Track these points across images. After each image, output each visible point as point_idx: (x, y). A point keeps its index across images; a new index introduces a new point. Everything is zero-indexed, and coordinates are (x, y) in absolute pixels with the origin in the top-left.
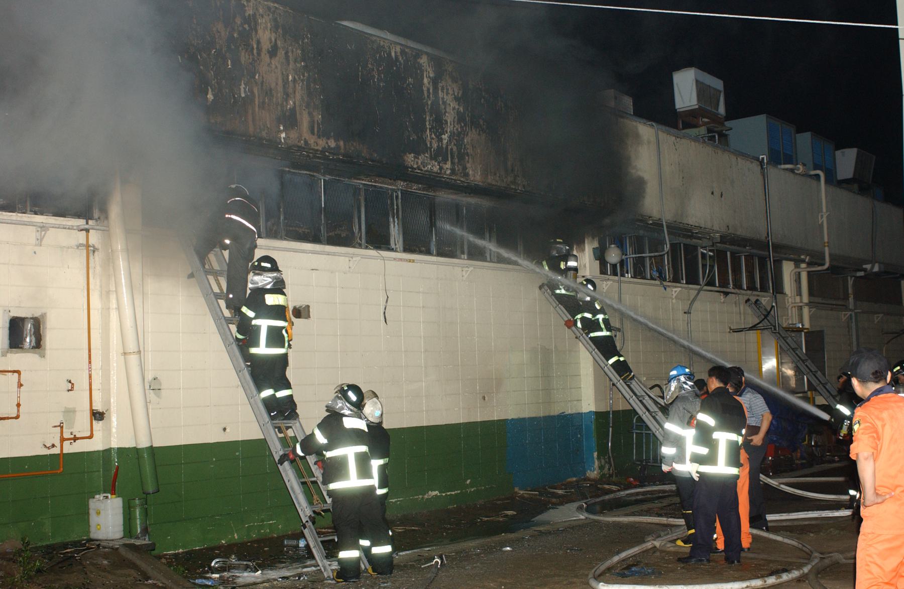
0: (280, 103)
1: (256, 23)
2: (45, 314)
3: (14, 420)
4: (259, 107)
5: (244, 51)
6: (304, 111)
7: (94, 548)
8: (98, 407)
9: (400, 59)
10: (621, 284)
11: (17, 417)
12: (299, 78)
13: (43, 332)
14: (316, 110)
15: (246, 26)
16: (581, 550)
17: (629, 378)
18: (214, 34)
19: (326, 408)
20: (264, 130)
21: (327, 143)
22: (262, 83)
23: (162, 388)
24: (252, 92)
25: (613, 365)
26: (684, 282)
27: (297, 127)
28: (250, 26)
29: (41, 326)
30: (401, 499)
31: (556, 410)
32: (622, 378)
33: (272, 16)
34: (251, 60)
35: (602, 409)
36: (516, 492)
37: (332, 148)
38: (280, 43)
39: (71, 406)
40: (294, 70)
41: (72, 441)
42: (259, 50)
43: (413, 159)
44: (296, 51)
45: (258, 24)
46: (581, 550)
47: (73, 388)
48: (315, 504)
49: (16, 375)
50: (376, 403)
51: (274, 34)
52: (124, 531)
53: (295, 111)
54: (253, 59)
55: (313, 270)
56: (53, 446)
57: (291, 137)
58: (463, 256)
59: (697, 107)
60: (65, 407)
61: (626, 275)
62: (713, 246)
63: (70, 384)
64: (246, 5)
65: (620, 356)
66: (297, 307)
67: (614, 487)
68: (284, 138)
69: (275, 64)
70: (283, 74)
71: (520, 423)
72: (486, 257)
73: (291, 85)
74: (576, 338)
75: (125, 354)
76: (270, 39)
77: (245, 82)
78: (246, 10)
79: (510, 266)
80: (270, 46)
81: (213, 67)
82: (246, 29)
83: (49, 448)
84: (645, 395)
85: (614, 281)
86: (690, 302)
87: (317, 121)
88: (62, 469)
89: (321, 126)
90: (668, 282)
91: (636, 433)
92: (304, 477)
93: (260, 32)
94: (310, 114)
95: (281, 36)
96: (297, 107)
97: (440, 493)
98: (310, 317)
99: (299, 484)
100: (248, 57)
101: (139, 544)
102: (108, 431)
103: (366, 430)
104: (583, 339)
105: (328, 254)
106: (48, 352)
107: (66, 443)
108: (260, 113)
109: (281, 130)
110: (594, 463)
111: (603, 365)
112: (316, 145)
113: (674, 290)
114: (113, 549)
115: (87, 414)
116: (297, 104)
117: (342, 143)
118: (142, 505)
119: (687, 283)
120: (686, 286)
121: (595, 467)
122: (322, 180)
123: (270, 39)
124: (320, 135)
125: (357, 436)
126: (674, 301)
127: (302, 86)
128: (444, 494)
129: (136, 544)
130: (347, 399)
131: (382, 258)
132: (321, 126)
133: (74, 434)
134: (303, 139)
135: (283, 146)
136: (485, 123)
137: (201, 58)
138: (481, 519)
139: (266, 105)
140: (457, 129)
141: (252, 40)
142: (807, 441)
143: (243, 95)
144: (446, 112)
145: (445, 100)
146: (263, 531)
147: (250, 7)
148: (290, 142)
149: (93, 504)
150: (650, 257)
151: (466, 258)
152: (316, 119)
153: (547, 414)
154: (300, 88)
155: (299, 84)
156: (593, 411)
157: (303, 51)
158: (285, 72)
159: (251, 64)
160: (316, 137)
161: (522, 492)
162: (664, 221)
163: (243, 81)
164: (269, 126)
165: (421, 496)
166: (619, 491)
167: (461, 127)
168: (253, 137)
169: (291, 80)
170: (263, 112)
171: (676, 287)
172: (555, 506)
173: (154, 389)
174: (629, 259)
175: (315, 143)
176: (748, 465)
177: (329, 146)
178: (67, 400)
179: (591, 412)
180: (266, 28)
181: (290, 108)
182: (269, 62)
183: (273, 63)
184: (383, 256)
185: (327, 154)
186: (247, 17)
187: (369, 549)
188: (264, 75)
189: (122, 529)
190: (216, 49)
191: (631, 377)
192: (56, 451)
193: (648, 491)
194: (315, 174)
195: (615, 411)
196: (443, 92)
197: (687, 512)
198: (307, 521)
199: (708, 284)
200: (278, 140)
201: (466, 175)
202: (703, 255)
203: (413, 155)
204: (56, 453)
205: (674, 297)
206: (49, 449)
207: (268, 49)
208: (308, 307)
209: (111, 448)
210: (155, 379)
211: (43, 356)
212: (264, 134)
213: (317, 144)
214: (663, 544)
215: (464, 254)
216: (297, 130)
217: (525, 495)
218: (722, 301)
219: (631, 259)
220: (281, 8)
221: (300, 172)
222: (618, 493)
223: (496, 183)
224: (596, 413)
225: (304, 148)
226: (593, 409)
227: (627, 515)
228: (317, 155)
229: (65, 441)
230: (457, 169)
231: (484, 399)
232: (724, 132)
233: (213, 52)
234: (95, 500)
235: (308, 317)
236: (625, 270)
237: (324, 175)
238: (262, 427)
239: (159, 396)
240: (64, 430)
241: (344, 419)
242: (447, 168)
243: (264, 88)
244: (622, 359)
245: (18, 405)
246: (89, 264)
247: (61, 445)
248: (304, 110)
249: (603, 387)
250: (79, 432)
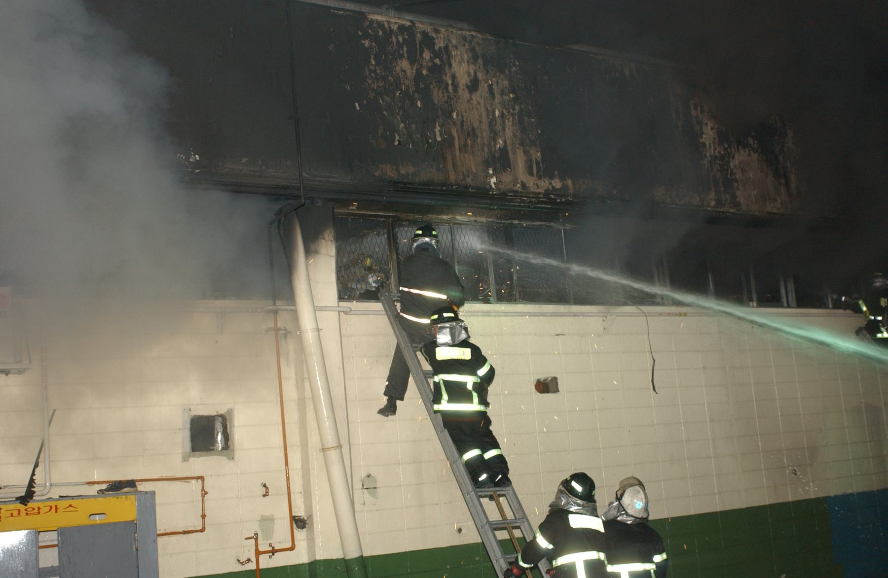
0: (486, 143)
1: (449, 55)
2: (232, 410)
3: (182, 535)
4: (460, 149)
6: (517, 150)
12: (509, 112)
13: (230, 432)
14: (534, 148)
15: (437, 61)
18: (398, 74)
21: (550, 184)
22: (463, 121)
23: (377, 486)
24: (450, 135)
27: (510, 168)
28: (441, 60)
29: (228, 424)
33: (469, 46)
38: (480, 75)
39: (268, 514)
40: (500, 103)
41: (271, 554)
42: (455, 86)
45: (452, 57)
47: (268, 493)
49: (200, 481)
50: (638, 492)
51: (473, 66)
54: (448, 97)
55: (557, 335)
56: (249, 560)
57: (504, 182)
58: (751, 303)
60: (262, 515)
63: (264, 488)
64: (435, 37)
66: (542, 380)
68: (494, 183)
69: (477, 100)
70: (487, 109)
72: (782, 302)
73: (499, 121)
75: (323, 450)
76: (468, 72)
77: (441, 124)
78: (435, 43)
80: (468, 80)
81: (399, 111)
82: (437, 64)
83: (242, 564)
87: (536, 159)
93: (455, 65)
94: (525, 152)
95: (481, 67)
96: (508, 146)
100: (442, 95)
102: (311, 540)
103: (602, 530)
106: (237, 454)
107: (262, 557)
108: (462, 157)
115: (287, 521)
116: (508, 143)
117: (569, 182)
123: (468, 72)
124: (540, 175)
125: (587, 539)
127: (513, 121)
130: (572, 491)
131: (643, 314)
133: (273, 546)
136: (755, 141)
140: (719, 152)
141: (446, 75)
142: (472, 191)
143: (439, 139)
144: (702, 133)
145: (700, 119)
147: (441, 39)
148: (503, 187)
151: (755, 305)
154: (510, 123)
155: (508, 119)
159: (446, 102)
160: (535, 178)
163: (437, 123)
164: (474, 171)
167: (725, 149)
168: (456, 185)
169: (499, 116)
177: (553, 187)
178: (266, 507)
180: (463, 60)
181: (499, 147)
182: (469, 98)
183: (474, 99)
184: (645, 312)
185: (552, 196)
186: (437, 51)
188: (464, 114)
190: (401, 90)
192: (252, 566)
194: (552, 224)
196: (697, 110)
200: (488, 187)
201: (737, 205)
206: (243, 565)
208: (555, 379)
209: (316, 560)
210: (368, 476)
212: (469, 181)
213: (538, 186)
215: (752, 301)
216: (511, 172)
220: (479, 35)
221: (533, 224)
225: (521, 192)
228: (541, 199)
229: (260, 554)
230: (724, 199)
231: (796, 474)
233: (398, 94)
235: (556, 390)
238: (480, 530)
239: (374, 496)
241: (571, 516)
242: (711, 199)
243: (465, 128)
248: (518, 148)
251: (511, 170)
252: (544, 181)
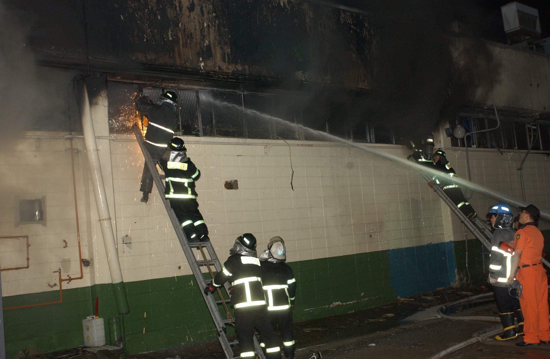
5: (169, 9)
7: (81, 354)
8: (86, 256)
9: (288, 7)
10: (468, 152)
11: (27, 267)
16: (423, 345)
17: (473, 217)
19: (230, 252)
20: (188, 61)
21: (236, 67)
24: (177, 37)
25: (461, 208)
26: (517, 148)
27: (212, 58)
29: (43, 205)
30: (313, 308)
31: (426, 241)
32: (468, 217)
34: (175, 14)
35: (460, 239)
36: (399, 299)
37: (239, 71)
41: (69, 281)
42: (181, 8)
43: (301, 74)
44: (209, 6)
46: (423, 345)
48: (228, 318)
49: (26, 239)
50: (280, 245)
52: (106, 340)
53: (211, 48)
54: (177, 14)
55: (238, 156)
56: (55, 285)
57: (208, 65)
59: (519, 28)
60: (63, 259)
61: (473, 146)
62: (535, 121)
63: (65, 243)
65: (466, 201)
67: (469, 293)
68: (203, 66)
69: (193, 16)
70: (199, 22)
71: (398, 252)
73: (206, 29)
74: (435, 191)
75: (100, 220)
77: (172, 30)
79: (327, 143)
80: (189, 4)
81: (147, 21)
83: (51, 287)
84: (485, 228)
85: (463, 151)
86: (521, 162)
87: (228, 53)
88: (62, 300)
89: (230, 56)
90: (505, 149)
91: (484, 254)
92: (221, 300)
94: (221, 48)
97: (341, 303)
98: (238, 188)
99: (215, 305)
100: (173, 12)
101: (112, 349)
102: (93, 273)
103: (259, 265)
104: (439, 191)
105: (249, 144)
107: (63, 283)
108: (184, 50)
109: (201, 61)
110: (455, 276)
111: (454, 209)
112: (227, 69)
113: (509, 154)
114: (94, 354)
116: (211, 43)
117: (247, 67)
118: (117, 322)
119: (518, 149)
120: (518, 151)
121: (456, 279)
122: (242, 95)
125: (251, 270)
126: (510, 162)
128: (344, 304)
129: (109, 349)
131: (288, 145)
132: (230, 56)
133: (70, 276)
134: (217, 66)
135: (203, 72)
137: (138, 15)
138: (368, 321)
139: (188, 44)
146: (212, 335)
148: (208, 68)
149: (85, 323)
150: (490, 132)
152: (226, 52)
153: (419, 245)
154: (213, 31)
156: (453, 241)
157: (213, 5)
158: (202, 21)
159: (175, 17)
160: (227, 64)
161: (402, 300)
162: (495, 107)
163: (170, 29)
164: (191, 59)
165: (327, 306)
166: (472, 295)
169: (206, 26)
170: (186, 49)
171: (510, 152)
172: (424, 308)
174: (474, 134)
175: (227, 68)
176: (547, 278)
177: (237, 70)
179: (451, 241)
181: (206, 45)
183: (192, 15)
187: (264, 349)
188: (186, 24)
189: (105, 339)
190: (149, 9)
191: (475, 216)
192: (57, 288)
193: (486, 296)
194: (236, 91)
195: (469, 240)
197: (503, 314)
198: (221, 331)
199: (533, 148)
200: (199, 68)
202: (529, 129)
203: (301, 72)
204: (58, 290)
205: (509, 159)
207: (188, 6)
208: (236, 181)
209: (95, 285)
210: (126, 236)
211: (45, 225)
214: (484, 339)
217: (404, 301)
218: (546, 160)
219: (476, 135)
221: (225, 90)
222: (470, 297)
223: (366, 88)
224: (455, 242)
225: (219, 72)
226: (453, 240)
227: (471, 315)
228: (230, 76)
232: (541, 44)
234: (86, 320)
235: (237, 188)
236: (472, 142)
237: (242, 91)
238: (191, 266)
240: (62, 274)
241: (242, 258)
243: (186, 33)
244: (467, 204)
245: (28, 259)
247: (60, 284)
248: (217, 46)
249: (457, 222)
250: (74, 274)
251: (213, 59)
252: (232, 66)
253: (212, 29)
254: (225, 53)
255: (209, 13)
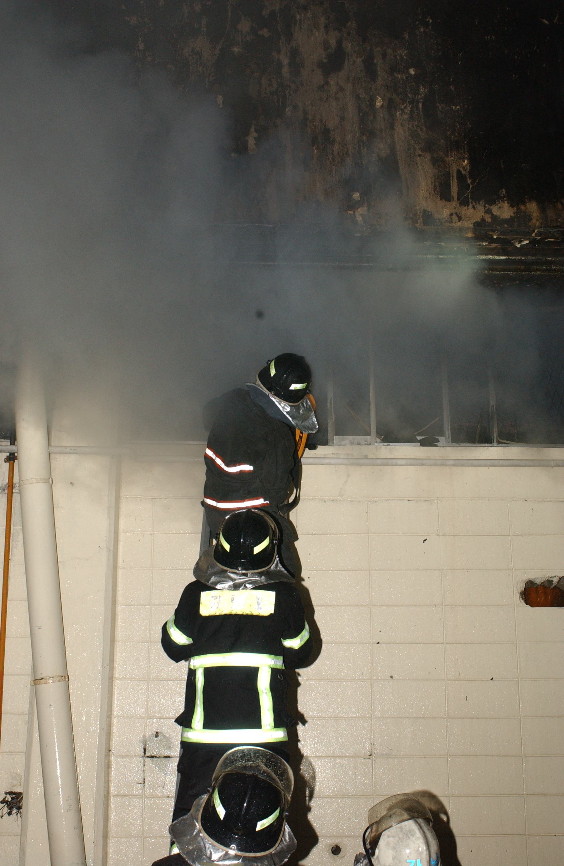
6: (419, 158)
21: (488, 211)
50: (409, 834)
87: (459, 172)
160: (455, 203)
173: (153, 757)
177: (494, 217)
183: (332, 83)
246: (6, 608)
248: (420, 156)
252: (474, 208)
253: (403, 110)
254: (449, 173)
255: (393, 69)
